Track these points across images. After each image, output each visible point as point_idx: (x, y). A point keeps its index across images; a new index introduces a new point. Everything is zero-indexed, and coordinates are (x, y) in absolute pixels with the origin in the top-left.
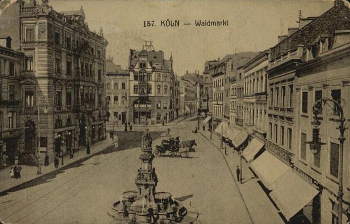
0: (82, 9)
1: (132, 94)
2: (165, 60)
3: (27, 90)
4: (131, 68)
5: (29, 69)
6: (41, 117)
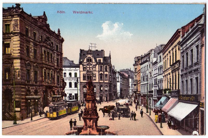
0: (44, 14)
1: (82, 81)
2: (106, 57)
3: (5, 69)
4: (81, 63)
5: (7, 53)
6: (16, 93)
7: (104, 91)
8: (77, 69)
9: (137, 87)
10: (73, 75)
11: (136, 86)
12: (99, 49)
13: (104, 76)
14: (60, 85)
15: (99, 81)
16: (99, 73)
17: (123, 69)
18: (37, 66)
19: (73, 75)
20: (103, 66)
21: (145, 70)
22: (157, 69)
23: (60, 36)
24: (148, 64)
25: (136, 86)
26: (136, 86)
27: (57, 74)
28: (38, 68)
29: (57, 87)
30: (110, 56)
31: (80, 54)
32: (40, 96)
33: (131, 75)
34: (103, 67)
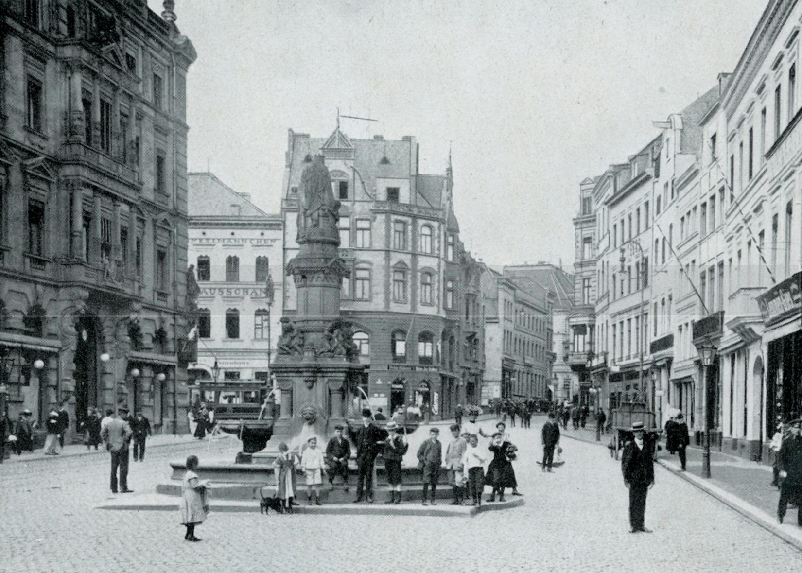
7: (417, 363)
8: (269, 234)
9: (590, 343)
10: (247, 272)
11: (585, 333)
12: (392, 135)
13: (414, 277)
14: (170, 299)
15: (387, 301)
16: (388, 258)
17: (522, 263)
18: (45, 173)
19: (247, 272)
20: (409, 220)
21: (634, 233)
22: (695, 208)
23: (176, 31)
24: (650, 198)
25: (585, 333)
26: (587, 337)
27: (155, 238)
28: (48, 183)
29: (151, 308)
30: (450, 170)
31: (287, 154)
32: (57, 343)
33: (561, 294)
34: (410, 228)
